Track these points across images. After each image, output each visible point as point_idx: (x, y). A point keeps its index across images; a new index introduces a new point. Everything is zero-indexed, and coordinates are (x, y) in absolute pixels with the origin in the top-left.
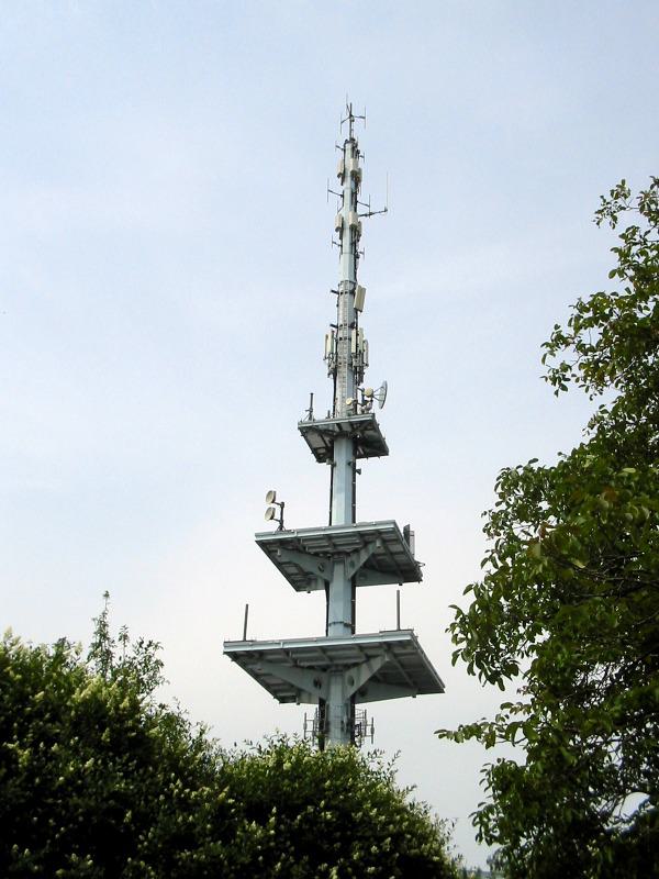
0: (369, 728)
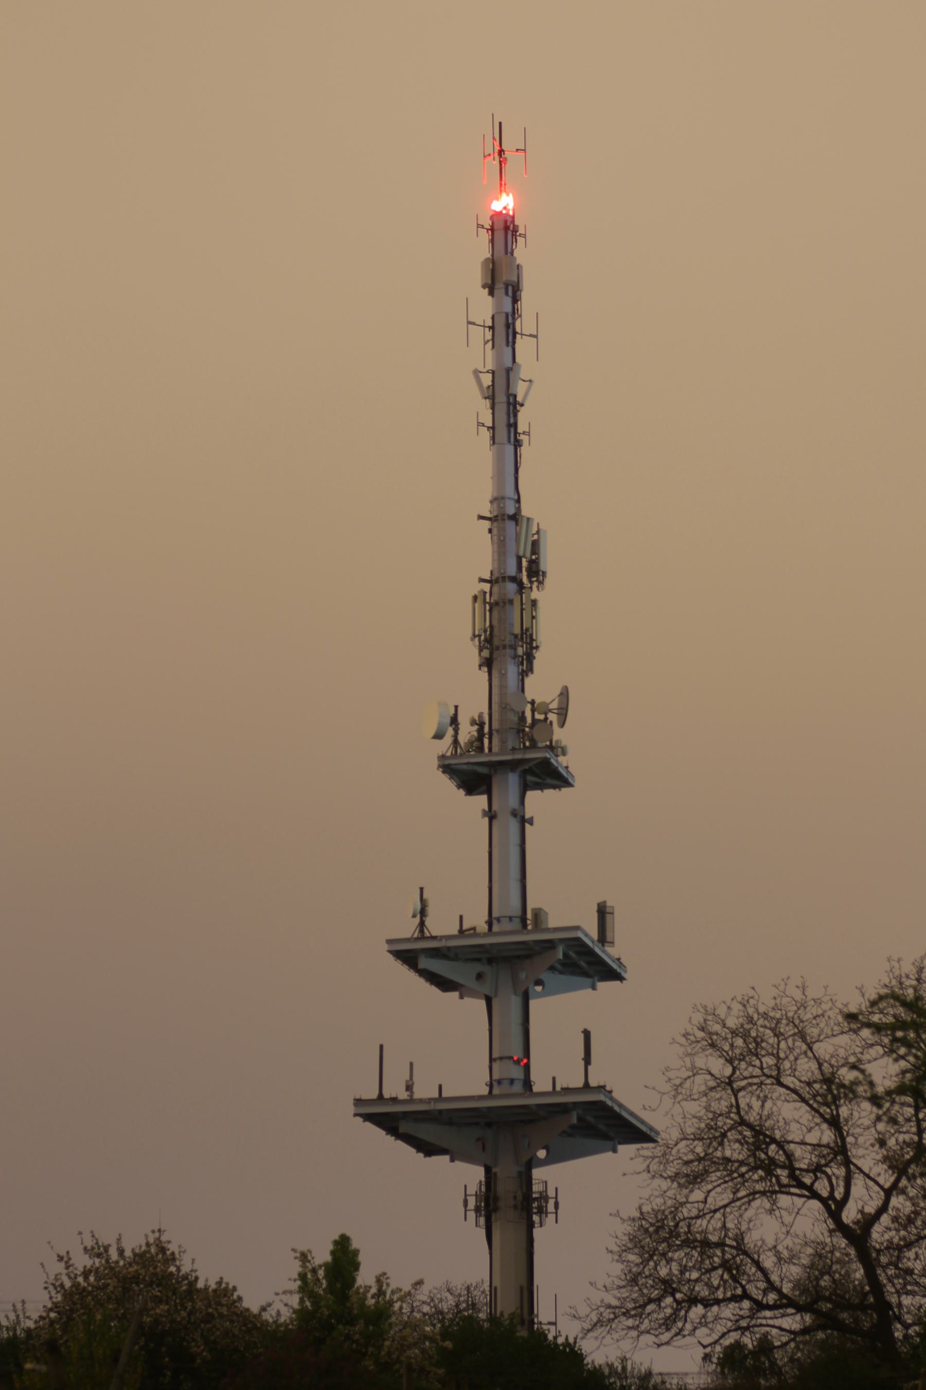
0: (551, 1203)
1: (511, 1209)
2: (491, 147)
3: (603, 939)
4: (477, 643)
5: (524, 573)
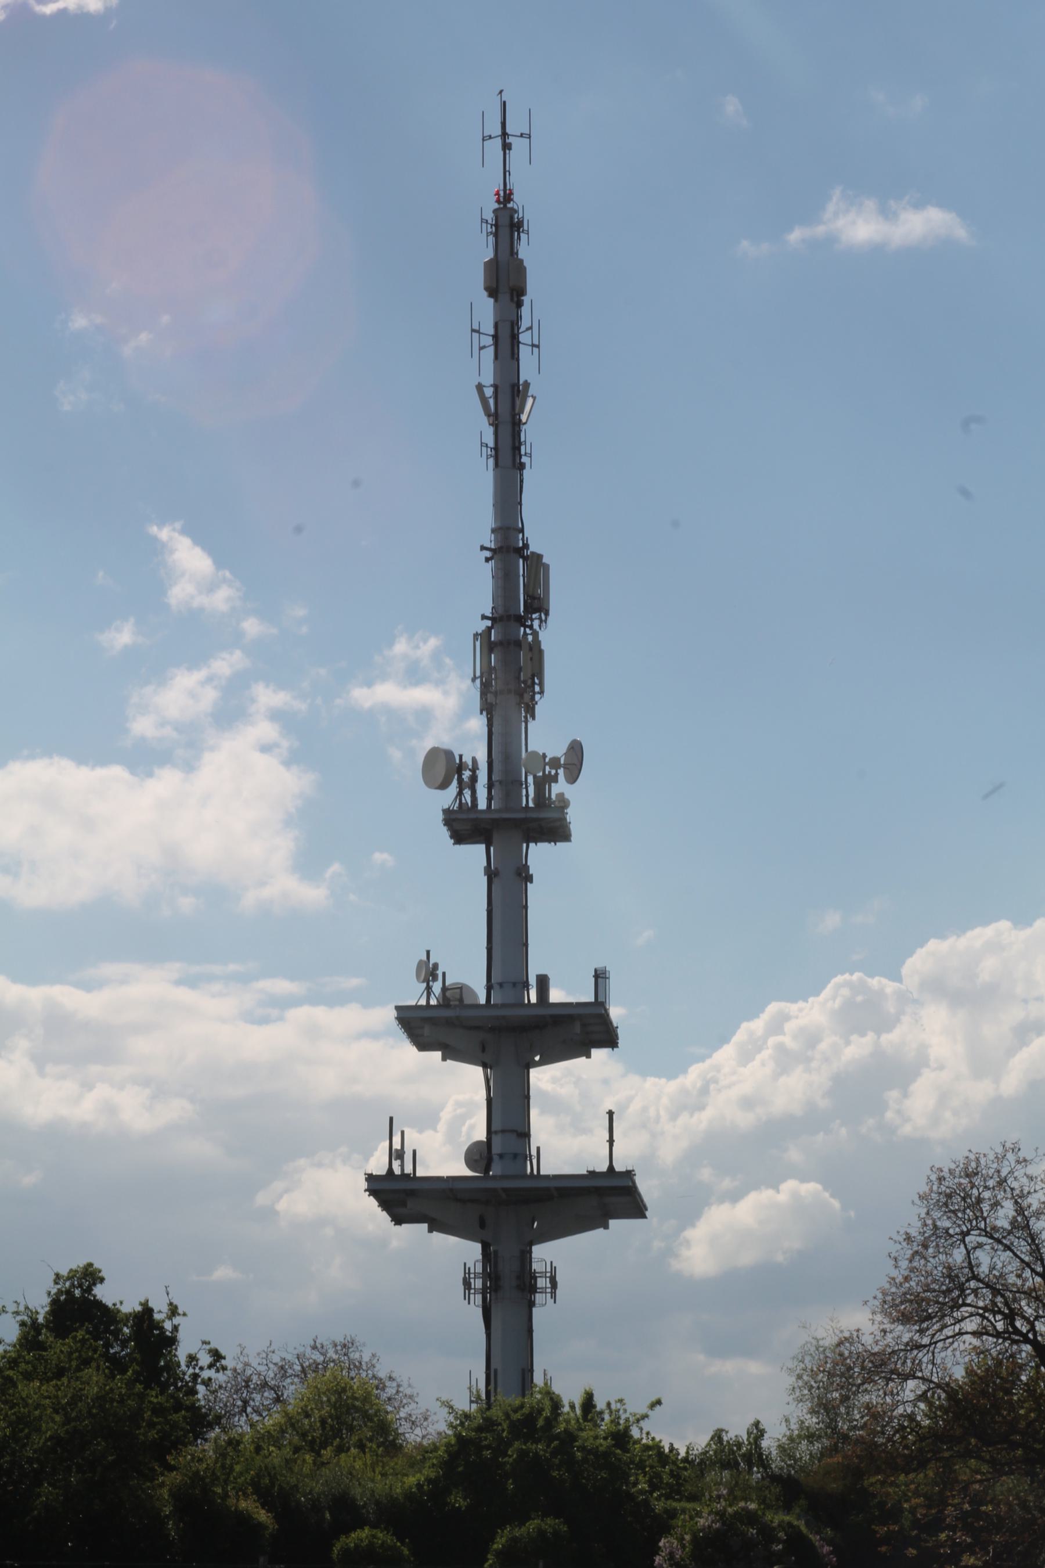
4: (479, 685)
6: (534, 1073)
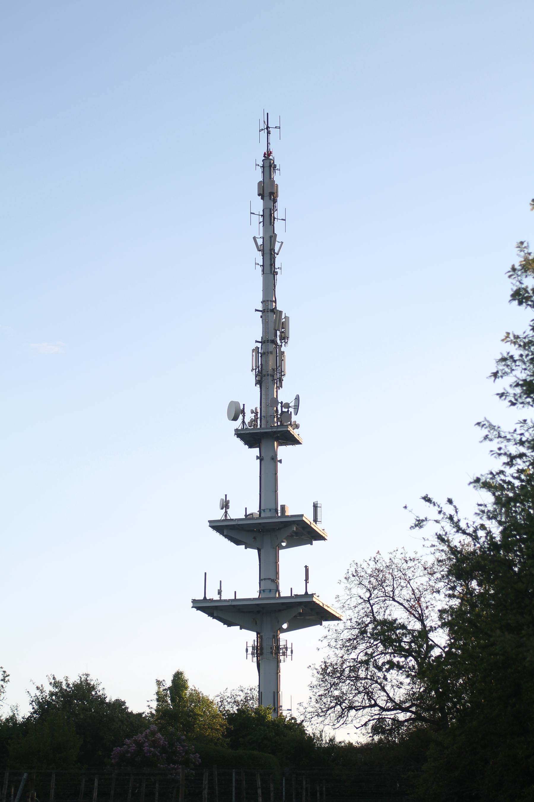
1: (268, 655)
2: (263, 126)
3: (315, 520)
5: (278, 338)
6: (282, 552)
